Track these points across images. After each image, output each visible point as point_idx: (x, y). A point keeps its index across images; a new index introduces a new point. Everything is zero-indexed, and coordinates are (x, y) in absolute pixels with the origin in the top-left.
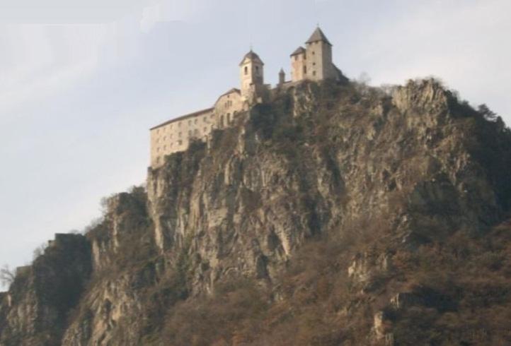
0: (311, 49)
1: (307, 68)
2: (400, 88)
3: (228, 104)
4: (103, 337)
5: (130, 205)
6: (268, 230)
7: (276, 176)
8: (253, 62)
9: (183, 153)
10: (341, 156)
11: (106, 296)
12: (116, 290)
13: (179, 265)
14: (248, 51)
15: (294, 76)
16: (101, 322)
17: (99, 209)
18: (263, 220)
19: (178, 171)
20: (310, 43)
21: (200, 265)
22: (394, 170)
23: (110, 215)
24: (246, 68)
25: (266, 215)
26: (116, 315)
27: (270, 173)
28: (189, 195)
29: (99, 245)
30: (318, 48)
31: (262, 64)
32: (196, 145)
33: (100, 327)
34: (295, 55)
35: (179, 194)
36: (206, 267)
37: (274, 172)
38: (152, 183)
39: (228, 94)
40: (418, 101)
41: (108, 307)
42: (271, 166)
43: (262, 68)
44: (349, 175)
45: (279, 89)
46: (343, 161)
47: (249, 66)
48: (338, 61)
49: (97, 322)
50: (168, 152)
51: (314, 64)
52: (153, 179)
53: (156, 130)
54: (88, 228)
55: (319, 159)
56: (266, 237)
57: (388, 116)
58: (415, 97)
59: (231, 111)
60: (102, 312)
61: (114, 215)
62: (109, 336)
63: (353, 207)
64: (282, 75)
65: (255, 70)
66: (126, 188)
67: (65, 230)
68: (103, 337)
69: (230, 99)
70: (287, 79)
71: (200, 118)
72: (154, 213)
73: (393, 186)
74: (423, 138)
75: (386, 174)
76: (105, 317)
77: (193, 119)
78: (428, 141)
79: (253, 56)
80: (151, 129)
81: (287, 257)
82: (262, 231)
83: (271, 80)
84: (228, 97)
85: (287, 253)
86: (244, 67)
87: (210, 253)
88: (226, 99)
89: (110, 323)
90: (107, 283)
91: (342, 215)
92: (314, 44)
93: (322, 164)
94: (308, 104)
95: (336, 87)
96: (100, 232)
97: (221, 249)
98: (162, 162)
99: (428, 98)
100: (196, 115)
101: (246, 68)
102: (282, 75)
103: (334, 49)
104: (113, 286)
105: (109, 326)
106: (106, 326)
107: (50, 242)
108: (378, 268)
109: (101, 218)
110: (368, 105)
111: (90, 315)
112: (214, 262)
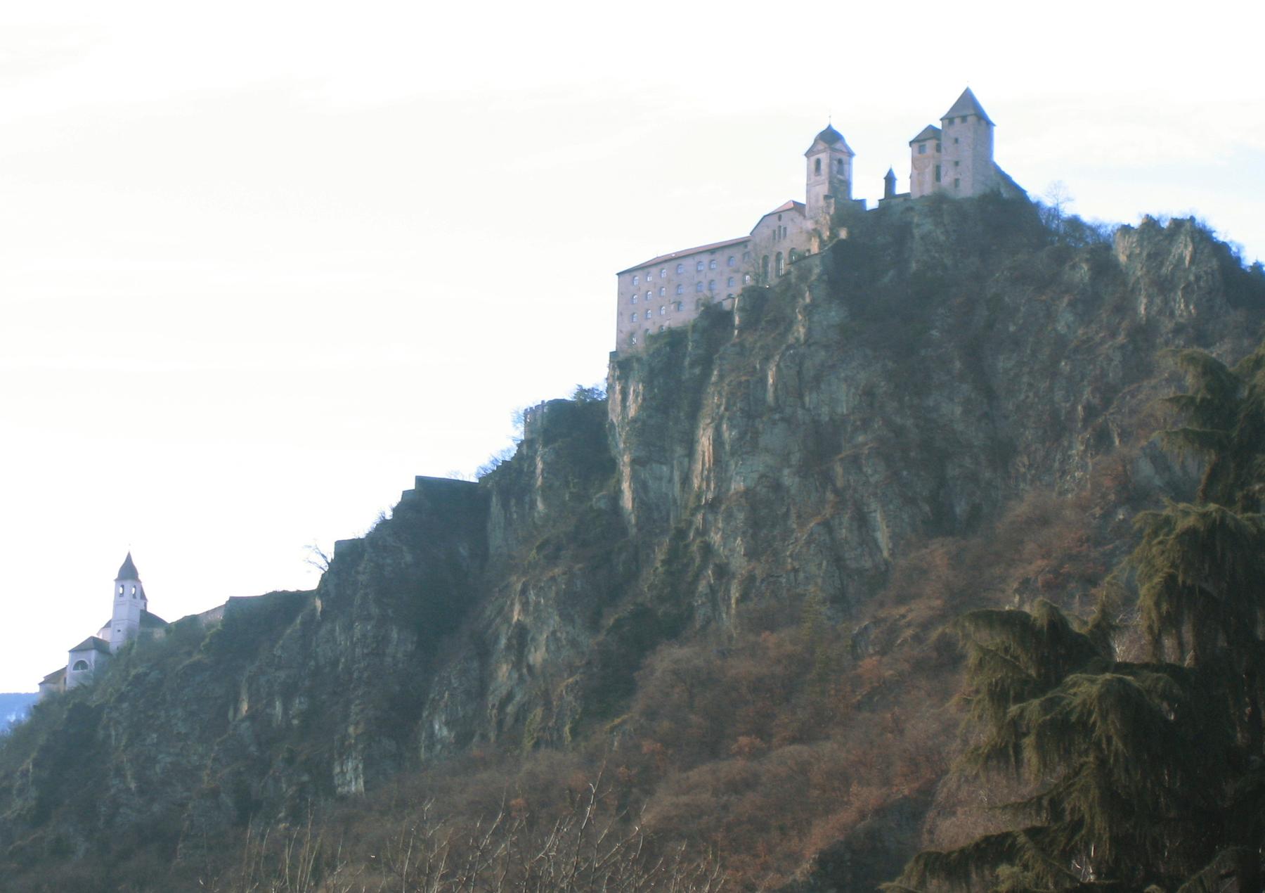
1: (943, 173)
18: (840, 483)
24: (818, 162)
26: (537, 656)
29: (505, 506)
31: (851, 154)
32: (715, 317)
33: (504, 672)
47: (824, 158)
51: (957, 164)
64: (890, 180)
71: (720, 257)
77: (705, 259)
79: (830, 138)
85: (886, 554)
86: (813, 159)
97: (754, 536)
101: (818, 162)
103: (997, 133)
111: (484, 651)
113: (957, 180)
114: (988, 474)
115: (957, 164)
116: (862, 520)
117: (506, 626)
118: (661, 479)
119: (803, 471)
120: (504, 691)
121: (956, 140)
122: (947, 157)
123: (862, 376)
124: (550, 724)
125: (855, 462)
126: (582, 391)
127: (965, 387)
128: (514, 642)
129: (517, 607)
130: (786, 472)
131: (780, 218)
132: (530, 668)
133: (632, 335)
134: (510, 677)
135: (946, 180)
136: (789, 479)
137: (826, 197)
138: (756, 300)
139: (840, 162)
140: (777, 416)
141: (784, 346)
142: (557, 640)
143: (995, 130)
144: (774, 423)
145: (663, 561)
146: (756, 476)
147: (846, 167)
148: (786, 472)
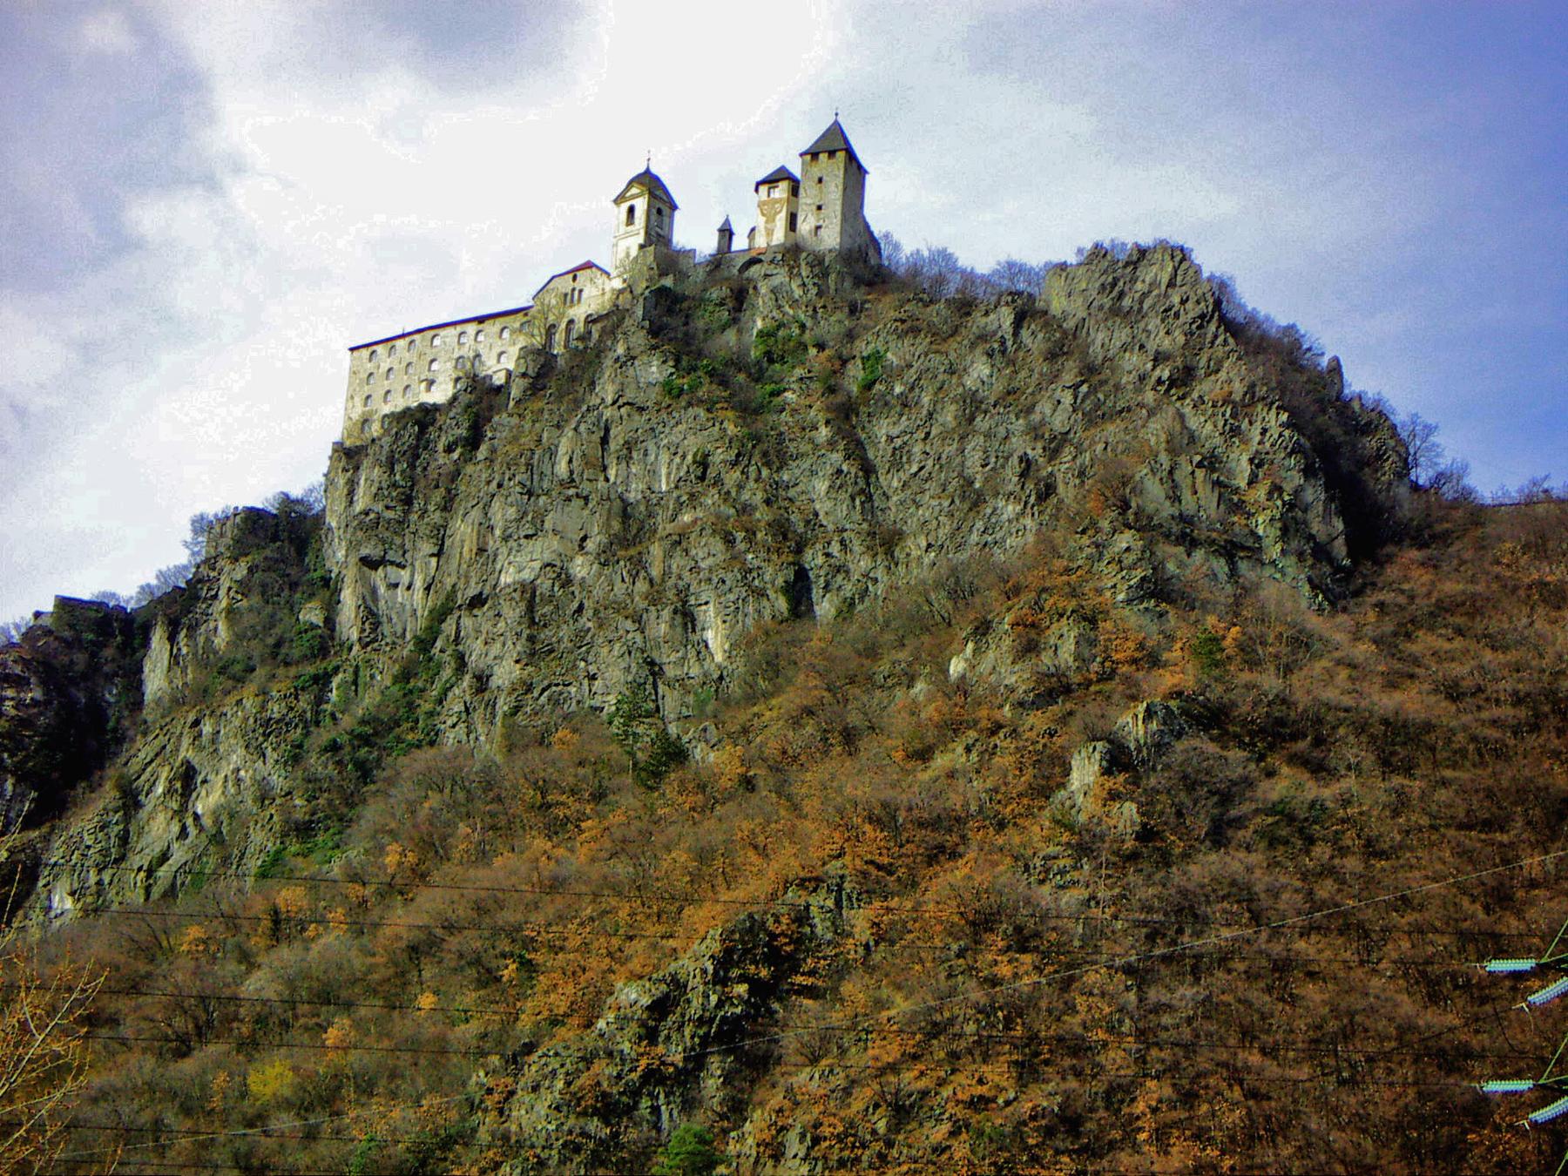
0: (816, 171)
1: (800, 220)
2: (1063, 267)
3: (569, 299)
4: (164, 857)
5: (274, 540)
6: (671, 594)
7: (703, 462)
8: (652, 195)
9: (436, 408)
10: (883, 429)
11: (186, 752)
12: (99, 883)
13: (405, 676)
14: (642, 170)
15: (757, 227)
16: (161, 818)
17: (186, 545)
18: (655, 572)
19: (418, 455)
20: (813, 154)
21: (467, 677)
22: (1053, 454)
23: (210, 562)
24: (631, 210)
25: (668, 555)
26: (206, 802)
27: (684, 457)
28: (447, 506)
29: (172, 638)
30: (833, 169)
31: (674, 207)
32: (481, 398)
33: (158, 828)
34: (771, 181)
35: (101, 945)
36: (482, 682)
37: (695, 455)
38: (341, 480)
39: (574, 273)
40: (1121, 295)
41: (188, 779)
42: (691, 440)
43: (671, 217)
44: (904, 476)
45: (718, 261)
46: (890, 439)
47: (641, 205)
48: (879, 213)
49: (151, 817)
50: (398, 404)
51: (819, 208)
52: (345, 470)
53: (365, 353)
54: (145, 589)
55: (824, 433)
56: (666, 614)
57: (1025, 334)
58: (1114, 284)
59: (579, 312)
60: (169, 791)
61: (221, 563)
62: (179, 854)
63: (915, 553)
64: (726, 233)
65: (654, 217)
66: (259, 494)
67: (84, 589)
68: (164, 857)
69: (578, 285)
70: (739, 243)
71: (492, 328)
72: (338, 554)
73: (1047, 491)
74: (1142, 378)
75: (1027, 465)
76: (175, 806)
77: (471, 328)
78: (1159, 382)
79: (649, 182)
80: (352, 350)
81: (719, 667)
82: (655, 599)
83: (694, 235)
84: (575, 278)
85: (719, 658)
86: (625, 206)
87: (496, 649)
88: (566, 284)
89: (190, 821)
90: (191, 717)
91: (880, 573)
92: (823, 157)
93: (832, 444)
94: (794, 303)
95: (863, 267)
96: (179, 604)
97: (531, 639)
98: (375, 429)
99: (1154, 284)
100: (481, 320)
101: (631, 210)
102: (726, 233)
103: (870, 180)
104: (207, 728)
105: (184, 829)
106: (175, 828)
107: (37, 615)
108: (1046, 658)
109: (185, 568)
110: (965, 306)
111: (131, 800)
112: (506, 673)
113: (818, 228)
114: (865, 563)
115: (819, 208)
116: (687, 618)
117: (167, 768)
118: (396, 586)
119: (605, 559)
120: (157, 850)
121: (820, 180)
122: (807, 198)
123: (692, 444)
124: (664, 488)
125: (679, 541)
126: (286, 500)
127: (836, 457)
128: (178, 785)
129: (186, 742)
130: (579, 560)
131: (575, 278)
132: (197, 817)
133: (366, 421)
134: (167, 830)
135: (805, 226)
136: (580, 568)
137: (642, 247)
138: (543, 372)
139: (659, 211)
140: (571, 492)
141: (584, 408)
142: (239, 780)
143: (868, 178)
144: (569, 499)
145: (761, 334)
146: (537, 565)
147: (666, 220)
148: (579, 560)
